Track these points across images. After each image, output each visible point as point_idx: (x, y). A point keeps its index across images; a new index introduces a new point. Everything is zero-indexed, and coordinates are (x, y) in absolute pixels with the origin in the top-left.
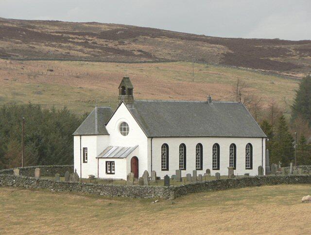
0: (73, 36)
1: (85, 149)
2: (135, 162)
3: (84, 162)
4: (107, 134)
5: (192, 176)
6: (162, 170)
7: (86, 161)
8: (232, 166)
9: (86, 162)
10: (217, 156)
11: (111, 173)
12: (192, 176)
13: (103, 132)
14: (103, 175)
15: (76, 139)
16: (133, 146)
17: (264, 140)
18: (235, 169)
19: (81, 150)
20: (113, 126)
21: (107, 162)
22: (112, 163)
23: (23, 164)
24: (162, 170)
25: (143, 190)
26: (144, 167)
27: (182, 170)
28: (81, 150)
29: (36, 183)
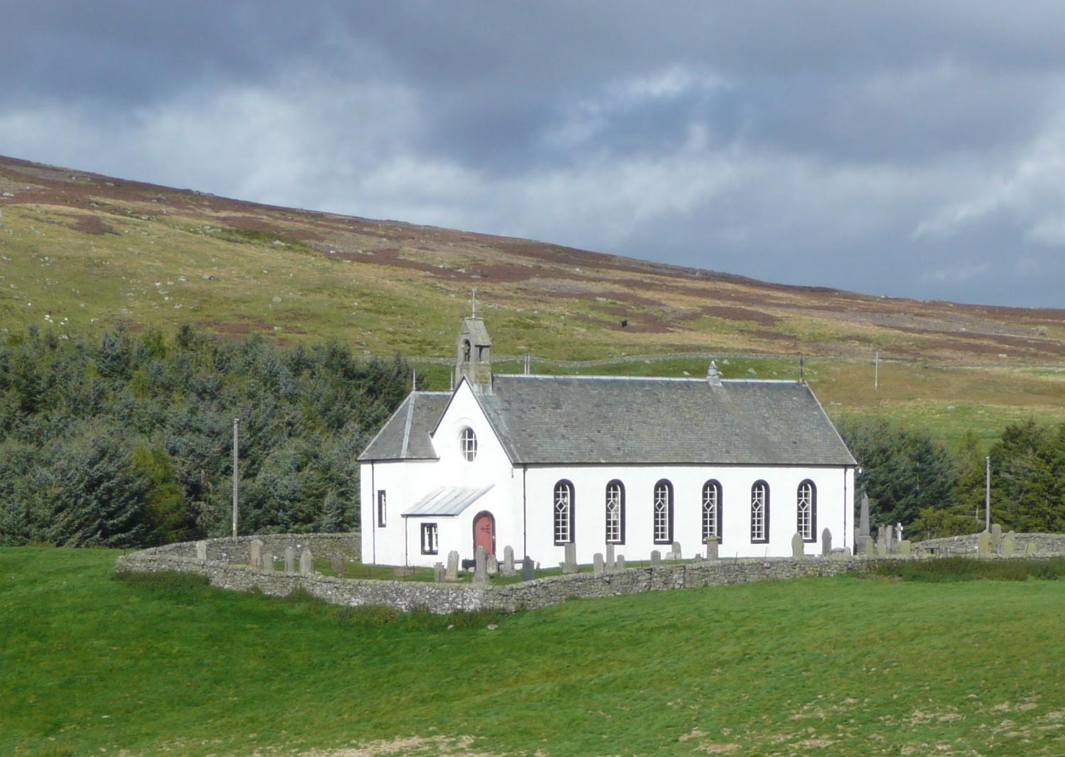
0: (671, 279)
1: (382, 493)
2: (485, 522)
3: (381, 525)
4: (433, 458)
5: (605, 560)
6: (753, 542)
7: (384, 522)
8: (615, 537)
9: (384, 526)
10: (715, 512)
11: (432, 552)
12: (605, 560)
13: (423, 454)
14: (419, 560)
15: (365, 469)
16: (484, 486)
17: (851, 471)
18: (720, 541)
19: (373, 495)
20: (445, 439)
21: (423, 525)
22: (431, 526)
23: (238, 528)
24: (767, 541)
25: (438, 595)
26: (506, 538)
27: (614, 543)
28: (373, 495)
29: (222, 574)
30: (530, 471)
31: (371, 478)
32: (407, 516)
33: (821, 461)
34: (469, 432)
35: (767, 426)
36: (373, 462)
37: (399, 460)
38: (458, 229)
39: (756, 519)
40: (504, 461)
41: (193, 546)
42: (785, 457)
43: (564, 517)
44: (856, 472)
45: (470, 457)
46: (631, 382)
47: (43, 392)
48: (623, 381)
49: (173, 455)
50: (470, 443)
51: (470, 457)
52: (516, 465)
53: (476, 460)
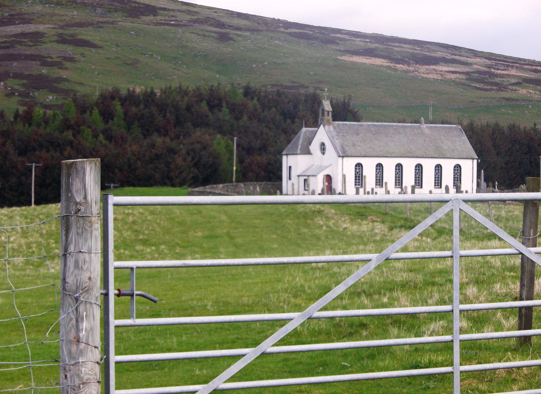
15: (284, 158)
17: (475, 162)
20: (315, 146)
30: (345, 159)
31: (287, 161)
32: (299, 176)
33: (393, 156)
34: (323, 144)
35: (442, 143)
36: (287, 155)
37: (297, 154)
38: (379, 33)
39: (437, 179)
40: (335, 155)
41: (217, 187)
42: (449, 155)
43: (359, 177)
44: (478, 161)
45: (323, 154)
46: (389, 126)
47: (157, 214)
48: (386, 125)
49: (20, 154)
50: (323, 148)
51: (323, 154)
52: (339, 156)
53: (326, 154)
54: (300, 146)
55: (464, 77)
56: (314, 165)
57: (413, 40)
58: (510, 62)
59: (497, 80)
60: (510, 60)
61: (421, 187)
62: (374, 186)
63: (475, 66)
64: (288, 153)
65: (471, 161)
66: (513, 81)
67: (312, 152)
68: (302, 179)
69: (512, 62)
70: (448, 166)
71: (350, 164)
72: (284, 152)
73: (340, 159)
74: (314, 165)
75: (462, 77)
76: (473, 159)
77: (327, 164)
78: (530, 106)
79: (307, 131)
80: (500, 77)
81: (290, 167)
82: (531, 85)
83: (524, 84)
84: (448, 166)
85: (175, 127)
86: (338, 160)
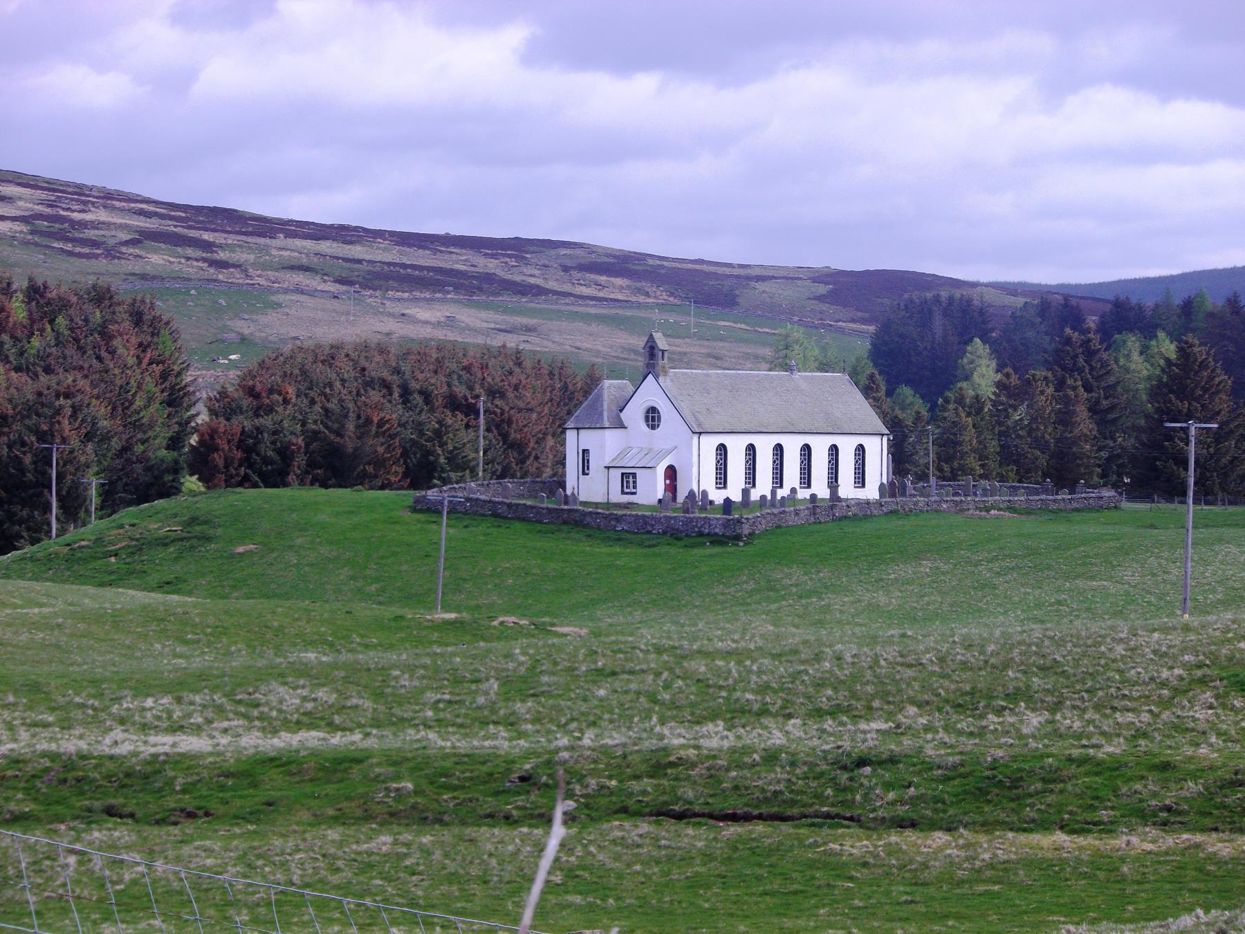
17: (885, 439)
20: (634, 414)
32: (608, 468)
44: (889, 440)
54: (605, 414)
55: (17, 227)
56: (632, 448)
57: (867, 273)
58: (70, 193)
59: (91, 234)
60: (70, 190)
61: (863, 486)
62: (797, 486)
63: (21, 203)
64: (580, 426)
65: (877, 439)
66: (125, 236)
67: (626, 425)
68: (616, 475)
69: (75, 193)
70: (847, 446)
71: (709, 444)
72: (569, 424)
73: (695, 438)
74: (632, 448)
75: (19, 229)
76: (883, 435)
77: (668, 447)
78: (193, 292)
79: (611, 384)
80: (94, 228)
81: (585, 452)
82: (163, 246)
83: (147, 243)
84: (847, 446)
85: (1220, 411)
86: (692, 439)
